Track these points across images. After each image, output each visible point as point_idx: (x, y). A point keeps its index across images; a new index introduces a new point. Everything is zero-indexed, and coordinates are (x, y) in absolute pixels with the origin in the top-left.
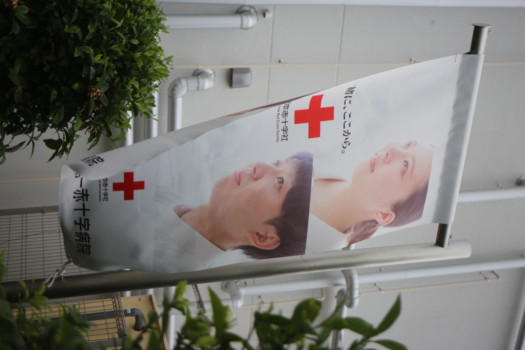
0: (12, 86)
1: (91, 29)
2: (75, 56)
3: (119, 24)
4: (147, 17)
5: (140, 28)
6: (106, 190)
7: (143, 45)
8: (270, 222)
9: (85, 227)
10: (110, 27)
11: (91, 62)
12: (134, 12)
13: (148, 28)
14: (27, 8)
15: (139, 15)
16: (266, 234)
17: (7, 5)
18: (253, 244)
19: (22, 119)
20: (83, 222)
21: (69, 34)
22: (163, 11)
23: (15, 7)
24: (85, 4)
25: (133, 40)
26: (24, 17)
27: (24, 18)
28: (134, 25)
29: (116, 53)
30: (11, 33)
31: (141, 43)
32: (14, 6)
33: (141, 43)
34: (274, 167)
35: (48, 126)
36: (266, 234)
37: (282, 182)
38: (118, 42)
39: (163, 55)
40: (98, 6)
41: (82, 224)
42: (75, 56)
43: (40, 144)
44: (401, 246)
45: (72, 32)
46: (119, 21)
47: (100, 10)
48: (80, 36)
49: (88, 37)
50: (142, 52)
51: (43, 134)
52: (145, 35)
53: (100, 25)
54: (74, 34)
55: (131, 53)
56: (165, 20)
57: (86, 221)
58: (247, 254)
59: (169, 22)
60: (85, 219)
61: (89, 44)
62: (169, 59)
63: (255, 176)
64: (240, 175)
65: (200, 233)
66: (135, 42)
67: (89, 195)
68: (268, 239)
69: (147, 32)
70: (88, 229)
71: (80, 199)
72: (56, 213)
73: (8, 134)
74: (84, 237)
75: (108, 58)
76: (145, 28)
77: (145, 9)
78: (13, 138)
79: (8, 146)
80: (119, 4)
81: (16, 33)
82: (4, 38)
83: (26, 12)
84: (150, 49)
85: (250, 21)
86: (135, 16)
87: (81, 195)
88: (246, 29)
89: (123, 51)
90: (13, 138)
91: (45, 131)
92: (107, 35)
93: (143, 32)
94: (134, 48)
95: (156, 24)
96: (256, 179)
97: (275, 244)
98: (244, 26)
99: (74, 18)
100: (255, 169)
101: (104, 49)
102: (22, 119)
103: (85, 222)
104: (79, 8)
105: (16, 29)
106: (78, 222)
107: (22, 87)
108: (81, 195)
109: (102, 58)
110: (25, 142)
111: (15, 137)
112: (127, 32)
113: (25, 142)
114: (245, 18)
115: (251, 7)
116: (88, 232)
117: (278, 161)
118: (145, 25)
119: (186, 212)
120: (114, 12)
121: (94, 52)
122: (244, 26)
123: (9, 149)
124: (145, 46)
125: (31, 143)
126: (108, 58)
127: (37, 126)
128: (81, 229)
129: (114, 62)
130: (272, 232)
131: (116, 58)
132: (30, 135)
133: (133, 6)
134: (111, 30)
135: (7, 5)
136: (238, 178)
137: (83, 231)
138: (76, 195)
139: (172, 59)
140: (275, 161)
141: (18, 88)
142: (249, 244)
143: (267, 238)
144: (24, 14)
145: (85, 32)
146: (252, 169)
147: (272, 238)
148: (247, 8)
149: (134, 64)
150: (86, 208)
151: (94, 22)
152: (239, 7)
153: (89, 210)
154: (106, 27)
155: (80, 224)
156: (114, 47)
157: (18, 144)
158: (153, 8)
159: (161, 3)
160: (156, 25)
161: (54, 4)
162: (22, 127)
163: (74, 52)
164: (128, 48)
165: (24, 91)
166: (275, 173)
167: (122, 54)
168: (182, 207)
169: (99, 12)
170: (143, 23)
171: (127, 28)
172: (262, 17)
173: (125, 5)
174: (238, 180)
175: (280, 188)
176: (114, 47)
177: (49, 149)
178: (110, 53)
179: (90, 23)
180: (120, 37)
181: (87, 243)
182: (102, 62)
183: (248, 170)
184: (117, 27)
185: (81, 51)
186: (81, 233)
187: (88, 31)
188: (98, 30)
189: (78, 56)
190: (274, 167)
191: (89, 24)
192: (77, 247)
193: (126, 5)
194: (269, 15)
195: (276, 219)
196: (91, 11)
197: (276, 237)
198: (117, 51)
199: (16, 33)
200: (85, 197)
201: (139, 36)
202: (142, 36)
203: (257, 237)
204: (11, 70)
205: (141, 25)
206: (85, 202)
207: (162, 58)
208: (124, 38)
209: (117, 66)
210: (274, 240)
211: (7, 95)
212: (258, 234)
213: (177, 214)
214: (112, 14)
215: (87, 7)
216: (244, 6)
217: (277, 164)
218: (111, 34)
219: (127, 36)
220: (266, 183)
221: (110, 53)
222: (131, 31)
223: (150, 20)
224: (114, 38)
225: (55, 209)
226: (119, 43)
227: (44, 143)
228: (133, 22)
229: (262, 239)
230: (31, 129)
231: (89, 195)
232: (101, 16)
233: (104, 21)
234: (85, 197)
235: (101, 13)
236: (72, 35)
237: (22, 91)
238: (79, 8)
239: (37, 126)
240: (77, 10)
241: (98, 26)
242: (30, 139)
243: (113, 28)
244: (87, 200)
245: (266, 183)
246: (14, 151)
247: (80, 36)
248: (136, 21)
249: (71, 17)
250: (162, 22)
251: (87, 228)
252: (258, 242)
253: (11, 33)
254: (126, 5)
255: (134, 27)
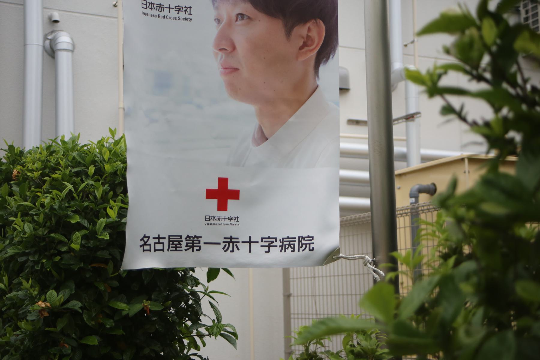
0: (143, 311)
1: (76, 219)
2: (108, 238)
3: (70, 186)
4: (60, 155)
5: (75, 163)
6: (225, 218)
7: (96, 161)
8: (289, 33)
9: (272, 242)
10: (73, 198)
11: (116, 221)
12: (54, 170)
13: (75, 154)
14: (50, 292)
15: (58, 164)
16: (303, 38)
17: (46, 314)
18: (314, 53)
19: (183, 304)
20: (267, 244)
21: (82, 246)
22: (53, 139)
23: (48, 304)
24: (44, 226)
25: (89, 173)
26: (61, 295)
27: (61, 295)
28: (71, 171)
29: (105, 193)
30: (81, 311)
31: (94, 162)
32: (47, 306)
33: (94, 162)
34: (221, 25)
35: (191, 276)
36: (303, 38)
37: (241, 16)
38: (91, 190)
39: (108, 139)
40: (47, 210)
41: (269, 244)
42: (108, 238)
43: (213, 285)
44: (73, 77)
45: (79, 241)
46: (67, 186)
47: (52, 208)
48: (84, 232)
49: (86, 223)
50: (104, 163)
51: (200, 281)
52: (83, 159)
53: (70, 210)
54: (82, 240)
55: (105, 176)
56: (63, 137)
57: (264, 240)
58: (328, 59)
59: (66, 132)
60: (262, 241)
61: (95, 224)
62: (113, 133)
63: (229, 49)
64: (226, 68)
65: (290, 116)
66: (92, 170)
67: (231, 236)
68: (310, 34)
69: (80, 155)
70: (276, 239)
71: (236, 246)
72: (291, 270)
73: (200, 320)
74: (288, 243)
75: (112, 202)
76: (74, 158)
77: (51, 157)
78: (205, 315)
79: (214, 321)
80: (44, 187)
81: (80, 305)
82: (85, 319)
83: (54, 293)
84: (101, 153)
85: (64, 40)
86: (59, 170)
87: (231, 244)
88: (74, 46)
89: (103, 184)
90: (205, 315)
91: (216, 277)
92: (83, 202)
93: (79, 160)
94: (99, 172)
95: (70, 146)
96: (234, 48)
97: (318, 26)
98: (70, 47)
99: (63, 238)
100: (221, 50)
101: (100, 206)
102: (183, 304)
103: (265, 242)
104: (50, 232)
105: (76, 305)
106: (267, 249)
107: (144, 301)
108: (231, 244)
109: (111, 208)
110: (210, 302)
111: (204, 313)
112: (80, 178)
113: (210, 302)
114: (60, 46)
115: (45, 38)
116: (279, 238)
117: (215, 20)
118: (70, 158)
119: (262, 132)
120: (55, 192)
121: (104, 218)
122: (70, 47)
123: (218, 320)
124: (96, 159)
125: (211, 294)
126: (112, 202)
127: (192, 287)
128: (276, 246)
129: (115, 195)
130: (302, 30)
131: (111, 193)
132: (201, 295)
133: (47, 171)
134: (77, 198)
135: (46, 314)
136: (229, 70)
137: (278, 244)
138: (231, 249)
139: (113, 129)
140: (215, 24)
141: (146, 306)
142: (314, 58)
143: (308, 36)
144: (58, 296)
145: (79, 227)
146: (220, 53)
147: (309, 30)
148: (48, 42)
149: (118, 172)
150: (248, 240)
151: (68, 216)
152: (45, 53)
153: (250, 237)
154: (72, 203)
155: (269, 246)
156: (98, 194)
157: (212, 309)
158: (49, 147)
159: (42, 141)
160: (71, 146)
161: (44, 261)
162: (192, 305)
163: (104, 239)
164: (100, 178)
165: (149, 299)
166: (229, 24)
167: (106, 186)
168: (256, 136)
169: (55, 209)
170: (68, 160)
171: (74, 178)
172: (59, 24)
173: (46, 181)
174: (231, 70)
175: (249, 18)
176: (98, 194)
177: (219, 276)
178: (105, 199)
179: (68, 220)
180: (85, 187)
181: (297, 240)
182: (116, 209)
183: (222, 57)
184: (73, 189)
185: (102, 233)
186: (282, 246)
187: (78, 223)
188: (76, 212)
189: (108, 236)
190: (221, 25)
191: (70, 222)
192: (303, 250)
193: (45, 178)
194: (56, 17)
195: (286, 25)
196: (53, 219)
197: (309, 25)
198: (103, 190)
199: (80, 305)
200: (233, 240)
201: (84, 165)
202: (84, 161)
203: (306, 49)
204: (124, 313)
205: (71, 162)
206: (239, 240)
207: (111, 141)
208: (86, 183)
209: (122, 193)
210: (312, 27)
211: (154, 319)
212: (301, 48)
213: (263, 142)
214: (57, 195)
215: (48, 224)
216: (44, 47)
217: (218, 21)
218: (82, 197)
219: (84, 179)
220: (241, 36)
221: (105, 199)
222: (77, 174)
223: (64, 152)
224: (87, 194)
225: (286, 272)
226: (93, 188)
227: (212, 282)
228: (67, 172)
229: (309, 43)
230: (194, 294)
231: (231, 236)
232: (60, 207)
233: (66, 205)
234: (233, 240)
235: (56, 207)
236: (83, 242)
237: (149, 301)
238: (50, 232)
239: (192, 287)
240: (53, 235)
241: (72, 211)
242: (206, 296)
243: (75, 195)
244: (237, 239)
245: (241, 36)
246: (220, 314)
247: (84, 232)
248: (66, 167)
249: (61, 242)
250: (66, 139)
251: (274, 240)
252: (312, 48)
253: (81, 311)
254: (45, 178)
255: (74, 170)
